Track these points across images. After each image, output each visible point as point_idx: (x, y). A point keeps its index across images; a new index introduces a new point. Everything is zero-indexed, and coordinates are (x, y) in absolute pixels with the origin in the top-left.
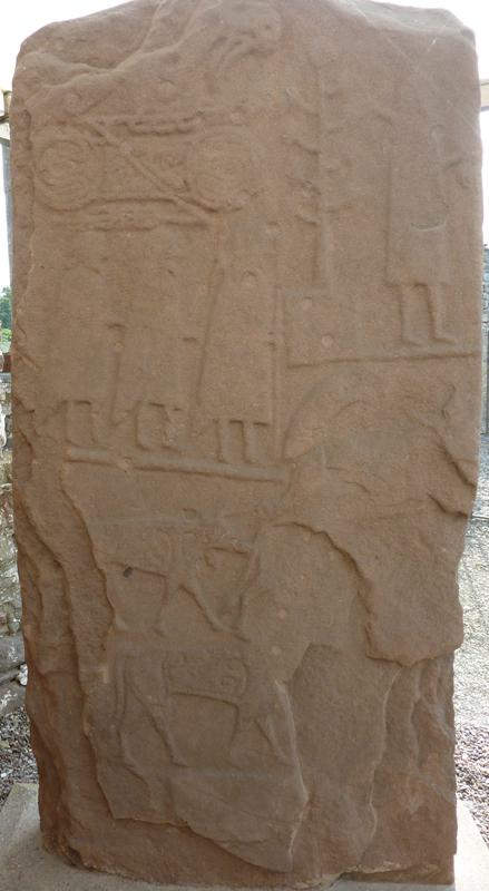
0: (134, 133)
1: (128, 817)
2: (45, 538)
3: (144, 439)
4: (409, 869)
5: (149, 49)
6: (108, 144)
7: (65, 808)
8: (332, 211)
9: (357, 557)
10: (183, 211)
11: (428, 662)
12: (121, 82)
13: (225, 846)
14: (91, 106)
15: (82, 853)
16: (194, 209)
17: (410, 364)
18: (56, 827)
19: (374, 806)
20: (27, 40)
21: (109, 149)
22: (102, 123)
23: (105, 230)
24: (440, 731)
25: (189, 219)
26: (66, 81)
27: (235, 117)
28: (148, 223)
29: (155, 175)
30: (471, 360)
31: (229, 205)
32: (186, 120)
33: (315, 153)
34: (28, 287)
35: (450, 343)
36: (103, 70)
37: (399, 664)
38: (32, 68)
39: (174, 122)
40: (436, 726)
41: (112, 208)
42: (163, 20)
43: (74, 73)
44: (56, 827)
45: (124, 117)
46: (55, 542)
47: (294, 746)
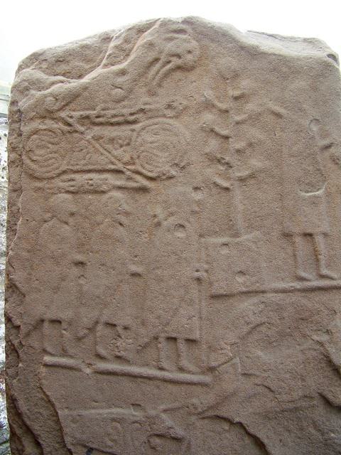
2: (28, 423)
3: (103, 352)
5: (106, 66)
6: (76, 131)
8: (241, 180)
9: (266, 441)
10: (129, 179)
12: (85, 88)
14: (64, 106)
16: (138, 178)
17: (303, 294)
21: (76, 135)
22: (71, 117)
23: (72, 193)
25: (135, 185)
27: (169, 113)
28: (105, 187)
31: (164, 175)
32: (132, 114)
33: (227, 138)
35: (332, 279)
36: (71, 81)
38: (25, 80)
39: (123, 115)
41: (77, 176)
42: (116, 47)
43: (53, 83)
45: (88, 112)
46: (36, 427)
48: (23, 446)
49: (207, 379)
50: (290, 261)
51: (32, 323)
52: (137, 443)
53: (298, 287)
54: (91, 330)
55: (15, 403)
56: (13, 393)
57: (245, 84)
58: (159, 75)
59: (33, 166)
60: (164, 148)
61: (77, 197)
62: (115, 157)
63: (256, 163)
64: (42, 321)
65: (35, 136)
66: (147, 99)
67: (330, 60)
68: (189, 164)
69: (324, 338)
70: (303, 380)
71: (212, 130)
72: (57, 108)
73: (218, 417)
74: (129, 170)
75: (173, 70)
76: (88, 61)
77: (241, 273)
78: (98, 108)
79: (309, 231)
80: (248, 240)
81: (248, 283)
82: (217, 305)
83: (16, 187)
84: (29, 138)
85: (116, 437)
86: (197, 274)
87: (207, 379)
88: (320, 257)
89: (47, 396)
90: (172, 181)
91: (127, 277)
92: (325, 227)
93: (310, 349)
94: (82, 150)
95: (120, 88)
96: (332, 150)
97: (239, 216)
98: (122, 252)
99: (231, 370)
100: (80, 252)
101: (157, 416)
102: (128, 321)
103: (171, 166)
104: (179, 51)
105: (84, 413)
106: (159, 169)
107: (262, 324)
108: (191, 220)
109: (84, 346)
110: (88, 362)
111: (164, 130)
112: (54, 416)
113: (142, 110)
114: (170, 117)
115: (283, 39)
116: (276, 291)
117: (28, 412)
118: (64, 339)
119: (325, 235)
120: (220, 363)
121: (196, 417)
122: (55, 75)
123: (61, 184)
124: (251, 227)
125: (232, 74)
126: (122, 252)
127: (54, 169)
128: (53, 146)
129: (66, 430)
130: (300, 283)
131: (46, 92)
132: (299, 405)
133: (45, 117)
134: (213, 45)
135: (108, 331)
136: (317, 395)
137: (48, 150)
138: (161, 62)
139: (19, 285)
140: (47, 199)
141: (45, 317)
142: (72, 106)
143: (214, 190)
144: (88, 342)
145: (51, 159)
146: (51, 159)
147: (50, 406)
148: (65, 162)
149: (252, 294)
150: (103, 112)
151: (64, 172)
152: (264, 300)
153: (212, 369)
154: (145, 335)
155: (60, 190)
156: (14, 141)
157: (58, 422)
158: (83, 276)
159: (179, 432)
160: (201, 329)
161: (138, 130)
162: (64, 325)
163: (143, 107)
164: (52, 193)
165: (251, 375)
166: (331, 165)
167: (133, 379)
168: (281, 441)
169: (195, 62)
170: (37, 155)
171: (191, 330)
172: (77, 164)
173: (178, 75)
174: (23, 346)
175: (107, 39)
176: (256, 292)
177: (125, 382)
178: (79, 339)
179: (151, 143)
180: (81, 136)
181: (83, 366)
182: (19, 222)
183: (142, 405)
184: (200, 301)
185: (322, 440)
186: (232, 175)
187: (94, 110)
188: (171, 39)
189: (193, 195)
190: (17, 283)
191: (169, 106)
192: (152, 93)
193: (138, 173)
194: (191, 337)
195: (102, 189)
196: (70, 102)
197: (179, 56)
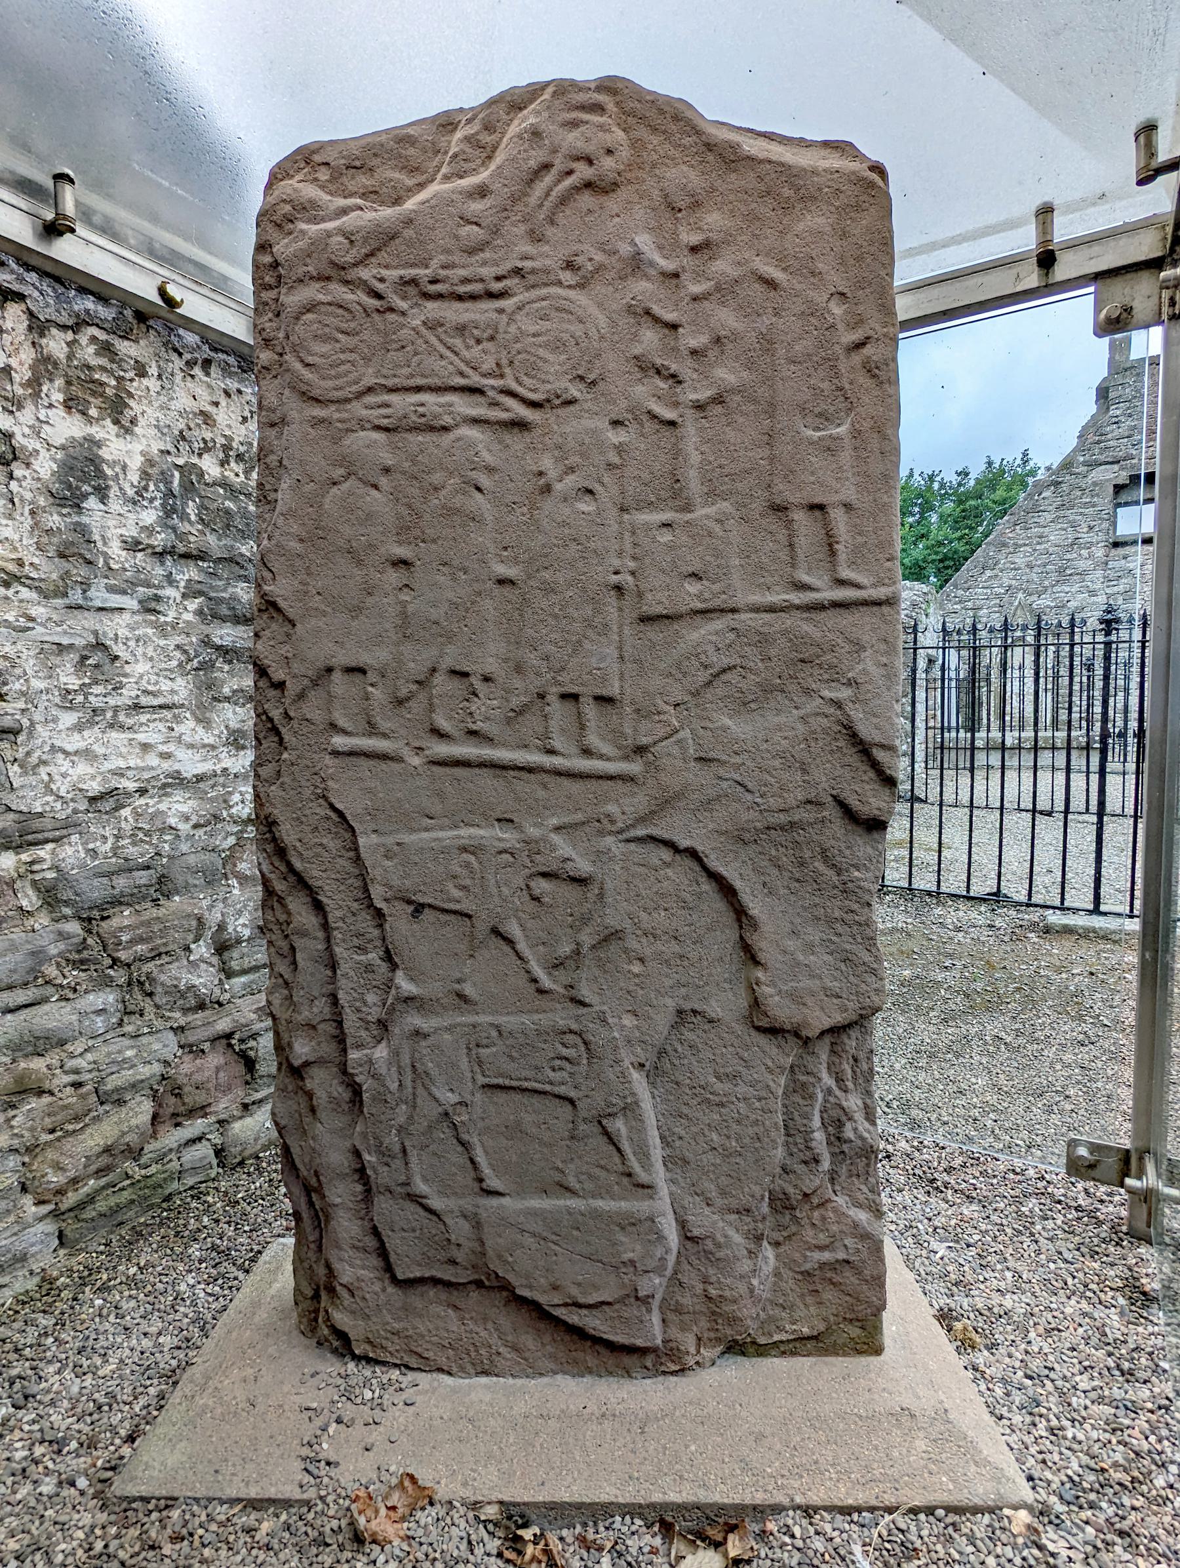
0: (427, 296)
2: (298, 865)
3: (444, 724)
5: (447, 178)
6: (391, 310)
8: (699, 407)
9: (738, 884)
10: (494, 404)
11: (836, 1031)
12: (409, 222)
14: (367, 256)
17: (805, 615)
18: (316, 1297)
20: (279, 165)
21: (391, 317)
22: (382, 280)
23: (387, 430)
25: (505, 416)
27: (567, 277)
28: (447, 420)
29: (456, 354)
30: (885, 609)
31: (558, 397)
32: (498, 279)
33: (674, 327)
35: (858, 586)
37: (797, 1035)
38: (284, 201)
39: (482, 280)
41: (394, 398)
42: (467, 139)
44: (316, 1297)
45: (413, 272)
46: (314, 873)
48: (289, 913)
49: (634, 767)
50: (784, 555)
51: (310, 673)
53: (797, 602)
55: (274, 829)
57: (714, 220)
58: (550, 199)
59: (307, 374)
60: (558, 346)
61: (396, 437)
63: (727, 375)
64: (330, 670)
66: (528, 249)
67: (874, 176)
69: (844, 694)
70: (805, 771)
71: (648, 312)
73: (653, 839)
75: (577, 189)
76: (413, 170)
78: (434, 263)
79: (817, 500)
80: (708, 517)
81: (707, 595)
82: (651, 635)
83: (275, 418)
84: (297, 318)
85: (468, 882)
86: (615, 579)
87: (634, 767)
88: (836, 546)
90: (572, 408)
91: (489, 584)
92: (849, 493)
93: (818, 714)
94: (403, 347)
95: (476, 224)
96: (867, 350)
97: (693, 473)
98: (482, 539)
99: (675, 751)
100: (400, 543)
101: (544, 839)
102: (491, 666)
103: (570, 381)
104: (590, 149)
105: (407, 838)
106: (549, 387)
107: (730, 668)
108: (606, 480)
109: (408, 716)
111: (557, 309)
112: (350, 849)
113: (517, 272)
114: (570, 287)
116: (756, 609)
117: (298, 844)
119: (848, 507)
120: (656, 738)
123: (364, 412)
124: (712, 495)
125: (688, 200)
126: (482, 539)
127: (350, 384)
128: (348, 339)
129: (375, 873)
130: (801, 595)
131: (330, 225)
132: (796, 818)
133: (328, 279)
134: (655, 140)
135: (455, 684)
136: (830, 799)
137: (338, 345)
138: (554, 171)
140: (336, 441)
141: (334, 662)
142: (383, 256)
143: (650, 426)
144: (416, 707)
145: (343, 363)
146: (343, 363)
148: (370, 370)
149: (712, 615)
150: (443, 273)
151: (370, 390)
152: (733, 624)
153: (640, 750)
154: (521, 690)
155: (362, 424)
157: (358, 860)
158: (407, 586)
159: (583, 866)
160: (622, 677)
161: (509, 311)
162: (372, 677)
164: (348, 430)
166: (863, 380)
167: (498, 772)
168: (764, 884)
171: (604, 679)
172: (395, 376)
173: (586, 200)
174: (291, 719)
175: (447, 123)
177: (485, 778)
178: (400, 702)
179: (534, 335)
180: (401, 319)
181: (406, 752)
182: (284, 486)
184: (621, 627)
186: (681, 398)
187: (427, 267)
188: (574, 124)
189: (609, 434)
192: (536, 237)
196: (379, 250)
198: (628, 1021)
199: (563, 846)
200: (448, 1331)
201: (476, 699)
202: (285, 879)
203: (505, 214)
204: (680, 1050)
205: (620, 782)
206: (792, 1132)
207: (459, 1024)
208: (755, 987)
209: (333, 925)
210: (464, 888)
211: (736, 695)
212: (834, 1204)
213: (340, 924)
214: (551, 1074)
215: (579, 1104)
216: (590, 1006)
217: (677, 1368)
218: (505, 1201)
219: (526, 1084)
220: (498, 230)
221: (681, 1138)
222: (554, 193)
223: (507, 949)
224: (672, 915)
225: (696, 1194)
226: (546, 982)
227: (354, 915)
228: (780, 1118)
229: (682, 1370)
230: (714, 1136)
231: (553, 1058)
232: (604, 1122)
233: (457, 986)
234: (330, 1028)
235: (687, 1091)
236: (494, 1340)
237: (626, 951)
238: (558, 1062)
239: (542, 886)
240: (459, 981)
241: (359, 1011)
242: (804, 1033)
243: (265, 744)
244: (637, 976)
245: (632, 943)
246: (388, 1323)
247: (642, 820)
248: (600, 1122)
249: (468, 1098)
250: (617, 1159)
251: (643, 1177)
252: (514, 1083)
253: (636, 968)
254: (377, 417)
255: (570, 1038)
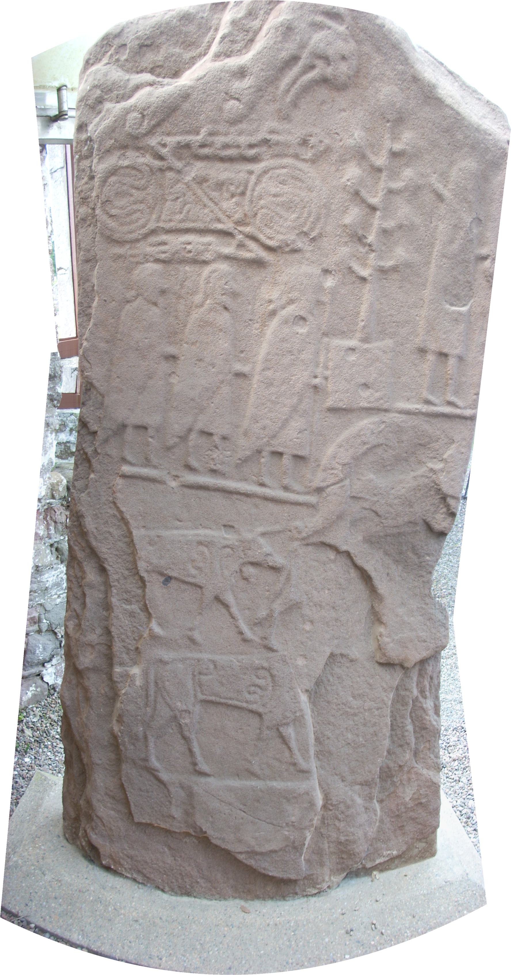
1: (149, 822)
2: (94, 543)
3: (194, 463)
4: (404, 853)
5: (217, 56)
6: (170, 169)
7: (89, 803)
9: (373, 574)
10: (241, 246)
11: (423, 662)
13: (241, 857)
15: (101, 850)
16: (252, 245)
17: (426, 419)
18: (77, 819)
19: (378, 801)
21: (170, 175)
22: (164, 146)
23: (163, 262)
24: (430, 721)
26: (130, 97)
28: (208, 256)
31: (288, 245)
32: (251, 146)
34: (92, 320)
36: (166, 80)
37: (402, 666)
39: (238, 147)
40: (427, 718)
43: (137, 88)
44: (77, 819)
46: (103, 550)
47: (312, 752)
49: (312, 499)
51: (113, 427)
52: (226, 573)
53: (424, 410)
54: (184, 438)
55: (81, 520)
56: (80, 508)
59: (112, 224)
62: (224, 212)
65: (113, 179)
68: (320, 235)
72: (144, 132)
74: (240, 232)
77: (366, 386)
79: (445, 350)
85: (201, 565)
86: (317, 381)
87: (312, 499)
89: (121, 512)
91: (230, 377)
100: (170, 343)
101: (254, 541)
103: (297, 235)
104: (330, 52)
105: (166, 533)
106: (281, 237)
109: (173, 457)
110: (175, 473)
111: (293, 177)
112: (126, 537)
113: (266, 142)
114: (304, 160)
115: (464, 86)
117: (95, 531)
118: (150, 448)
121: (299, 543)
122: (138, 73)
123: (149, 249)
129: (142, 553)
132: (402, 530)
134: (378, 58)
135: (203, 440)
136: (421, 521)
137: (132, 199)
138: (301, 63)
139: (97, 384)
140: (129, 271)
141: (128, 422)
142: (167, 127)
145: (135, 212)
146: (135, 212)
147: (123, 525)
148: (154, 216)
149: (373, 412)
151: (153, 232)
155: (146, 258)
156: (84, 187)
157: (131, 543)
159: (278, 560)
162: (151, 432)
163: (268, 137)
164: (137, 263)
165: (360, 498)
168: (388, 574)
169: (349, 78)
170: (117, 207)
173: (323, 93)
174: (98, 454)
176: (378, 410)
177: (218, 499)
178: (169, 449)
182: (95, 304)
183: (236, 526)
185: (417, 562)
190: (94, 381)
191: (304, 142)
193: (254, 238)
194: (300, 453)
195: (203, 258)
197: (326, 59)
198: (301, 662)
199: (266, 545)
200: (164, 862)
201: (216, 450)
202: (84, 551)
203: (260, 94)
204: (331, 680)
205: (305, 507)
206: (395, 728)
207: (189, 658)
208: (379, 638)
209: (112, 584)
210: (198, 568)
211: (380, 461)
212: (416, 769)
213: (116, 583)
214: (248, 696)
215: (265, 717)
216: (276, 651)
217: (316, 891)
218: (210, 780)
219: (230, 702)
220: (254, 106)
221: (328, 738)
222: (299, 83)
223: (224, 611)
224: (332, 592)
225: (336, 775)
226: (249, 634)
227: (125, 578)
228: (388, 720)
229: (319, 893)
230: (350, 736)
231: (250, 686)
232: (281, 729)
233: (190, 633)
234: (103, 649)
235: (334, 707)
236: (195, 873)
237: (302, 616)
238: (253, 688)
239: (250, 570)
240: (191, 629)
241: (123, 641)
242: (406, 665)
243: (80, 468)
244: (308, 632)
245: (306, 611)
246: (125, 849)
247: (317, 532)
248: (278, 729)
249: (191, 708)
250: (287, 753)
251: (303, 764)
252: (222, 701)
253: (308, 627)
254: (158, 253)
255: (261, 673)
